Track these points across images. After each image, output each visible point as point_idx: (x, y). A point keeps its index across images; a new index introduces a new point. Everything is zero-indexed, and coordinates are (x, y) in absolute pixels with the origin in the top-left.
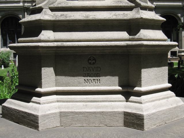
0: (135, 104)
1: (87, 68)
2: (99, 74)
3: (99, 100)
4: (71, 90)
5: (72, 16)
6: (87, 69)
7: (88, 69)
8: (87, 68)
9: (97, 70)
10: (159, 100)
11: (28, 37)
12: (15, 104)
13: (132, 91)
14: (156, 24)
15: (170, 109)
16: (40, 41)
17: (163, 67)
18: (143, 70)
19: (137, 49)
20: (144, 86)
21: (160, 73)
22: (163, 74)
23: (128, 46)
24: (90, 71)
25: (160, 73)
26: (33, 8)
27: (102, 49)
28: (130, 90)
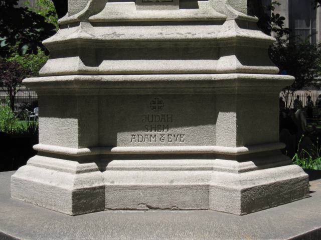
0: (118, 171)
1: (161, 116)
2: (159, 127)
3: (125, 167)
4: (68, 152)
5: (197, 33)
6: (161, 119)
7: (162, 119)
8: (161, 116)
9: (154, 120)
10: (48, 168)
11: (258, 66)
12: (289, 172)
13: (110, 153)
14: (70, 48)
15: (43, 186)
16: (99, 73)
17: (69, 119)
18: (75, 121)
19: (70, 87)
20: (119, 146)
21: (64, 128)
22: (69, 130)
23: (76, 81)
24: (165, 121)
25: (64, 128)
26: (249, 18)
27: (162, 86)
28: (104, 152)
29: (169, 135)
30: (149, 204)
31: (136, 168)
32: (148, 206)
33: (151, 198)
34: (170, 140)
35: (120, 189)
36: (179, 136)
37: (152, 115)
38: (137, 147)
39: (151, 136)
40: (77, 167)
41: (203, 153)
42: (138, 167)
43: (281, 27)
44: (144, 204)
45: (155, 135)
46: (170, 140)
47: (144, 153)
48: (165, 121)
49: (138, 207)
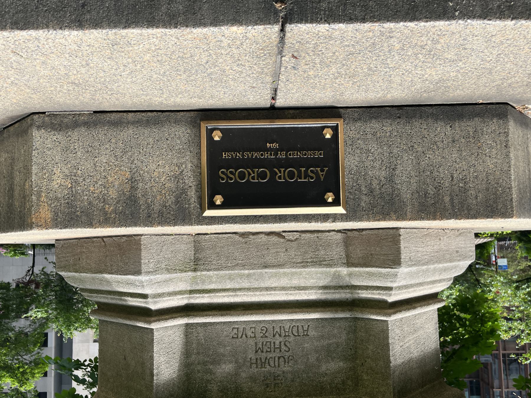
6: (267, 361)
9: (277, 359)
29: (255, 337)
30: (282, 240)
31: (302, 290)
32: (284, 237)
33: (278, 250)
34: (253, 330)
35: (324, 263)
36: (240, 335)
37: (279, 366)
38: (246, 320)
39: (280, 335)
40: (390, 295)
41: (304, 310)
42: (298, 292)
43: (15, 331)
44: (289, 240)
45: (274, 336)
46: (253, 330)
47: (291, 310)
48: (261, 358)
49: (297, 235)
